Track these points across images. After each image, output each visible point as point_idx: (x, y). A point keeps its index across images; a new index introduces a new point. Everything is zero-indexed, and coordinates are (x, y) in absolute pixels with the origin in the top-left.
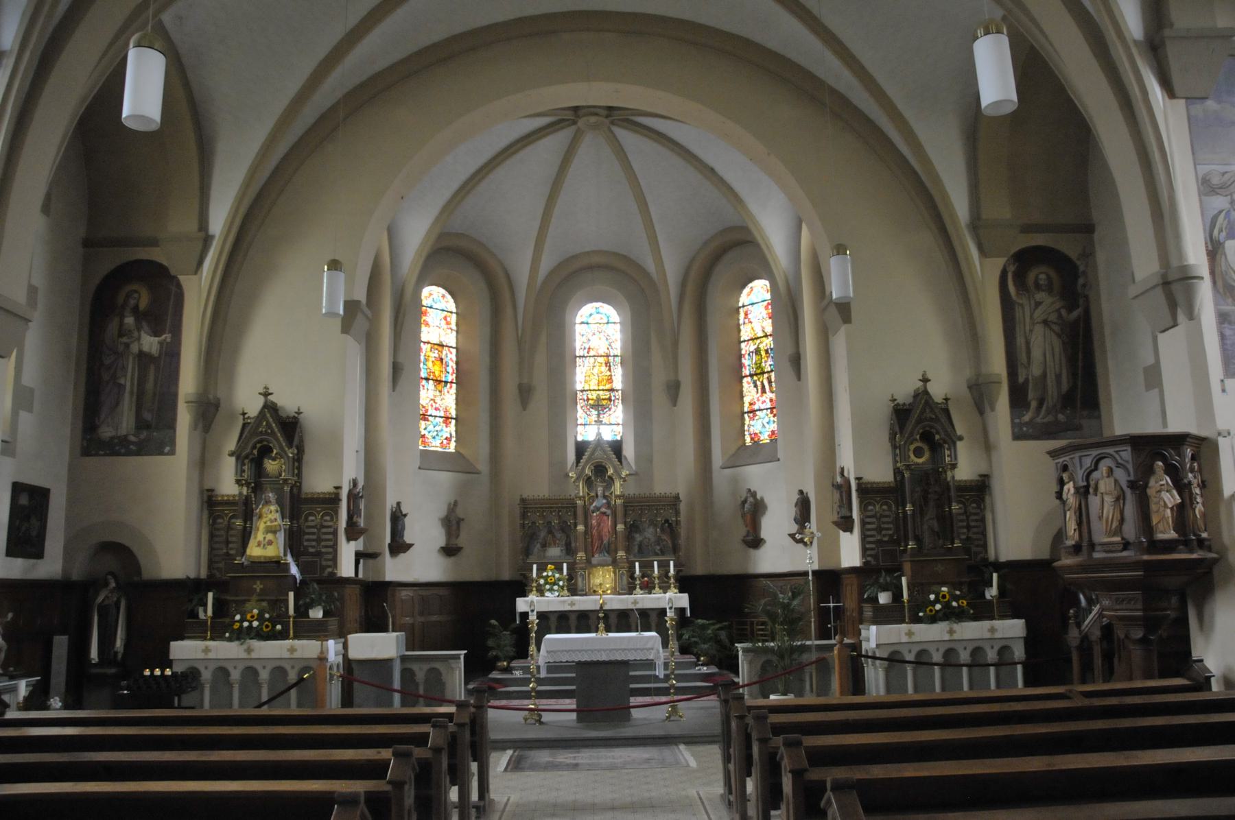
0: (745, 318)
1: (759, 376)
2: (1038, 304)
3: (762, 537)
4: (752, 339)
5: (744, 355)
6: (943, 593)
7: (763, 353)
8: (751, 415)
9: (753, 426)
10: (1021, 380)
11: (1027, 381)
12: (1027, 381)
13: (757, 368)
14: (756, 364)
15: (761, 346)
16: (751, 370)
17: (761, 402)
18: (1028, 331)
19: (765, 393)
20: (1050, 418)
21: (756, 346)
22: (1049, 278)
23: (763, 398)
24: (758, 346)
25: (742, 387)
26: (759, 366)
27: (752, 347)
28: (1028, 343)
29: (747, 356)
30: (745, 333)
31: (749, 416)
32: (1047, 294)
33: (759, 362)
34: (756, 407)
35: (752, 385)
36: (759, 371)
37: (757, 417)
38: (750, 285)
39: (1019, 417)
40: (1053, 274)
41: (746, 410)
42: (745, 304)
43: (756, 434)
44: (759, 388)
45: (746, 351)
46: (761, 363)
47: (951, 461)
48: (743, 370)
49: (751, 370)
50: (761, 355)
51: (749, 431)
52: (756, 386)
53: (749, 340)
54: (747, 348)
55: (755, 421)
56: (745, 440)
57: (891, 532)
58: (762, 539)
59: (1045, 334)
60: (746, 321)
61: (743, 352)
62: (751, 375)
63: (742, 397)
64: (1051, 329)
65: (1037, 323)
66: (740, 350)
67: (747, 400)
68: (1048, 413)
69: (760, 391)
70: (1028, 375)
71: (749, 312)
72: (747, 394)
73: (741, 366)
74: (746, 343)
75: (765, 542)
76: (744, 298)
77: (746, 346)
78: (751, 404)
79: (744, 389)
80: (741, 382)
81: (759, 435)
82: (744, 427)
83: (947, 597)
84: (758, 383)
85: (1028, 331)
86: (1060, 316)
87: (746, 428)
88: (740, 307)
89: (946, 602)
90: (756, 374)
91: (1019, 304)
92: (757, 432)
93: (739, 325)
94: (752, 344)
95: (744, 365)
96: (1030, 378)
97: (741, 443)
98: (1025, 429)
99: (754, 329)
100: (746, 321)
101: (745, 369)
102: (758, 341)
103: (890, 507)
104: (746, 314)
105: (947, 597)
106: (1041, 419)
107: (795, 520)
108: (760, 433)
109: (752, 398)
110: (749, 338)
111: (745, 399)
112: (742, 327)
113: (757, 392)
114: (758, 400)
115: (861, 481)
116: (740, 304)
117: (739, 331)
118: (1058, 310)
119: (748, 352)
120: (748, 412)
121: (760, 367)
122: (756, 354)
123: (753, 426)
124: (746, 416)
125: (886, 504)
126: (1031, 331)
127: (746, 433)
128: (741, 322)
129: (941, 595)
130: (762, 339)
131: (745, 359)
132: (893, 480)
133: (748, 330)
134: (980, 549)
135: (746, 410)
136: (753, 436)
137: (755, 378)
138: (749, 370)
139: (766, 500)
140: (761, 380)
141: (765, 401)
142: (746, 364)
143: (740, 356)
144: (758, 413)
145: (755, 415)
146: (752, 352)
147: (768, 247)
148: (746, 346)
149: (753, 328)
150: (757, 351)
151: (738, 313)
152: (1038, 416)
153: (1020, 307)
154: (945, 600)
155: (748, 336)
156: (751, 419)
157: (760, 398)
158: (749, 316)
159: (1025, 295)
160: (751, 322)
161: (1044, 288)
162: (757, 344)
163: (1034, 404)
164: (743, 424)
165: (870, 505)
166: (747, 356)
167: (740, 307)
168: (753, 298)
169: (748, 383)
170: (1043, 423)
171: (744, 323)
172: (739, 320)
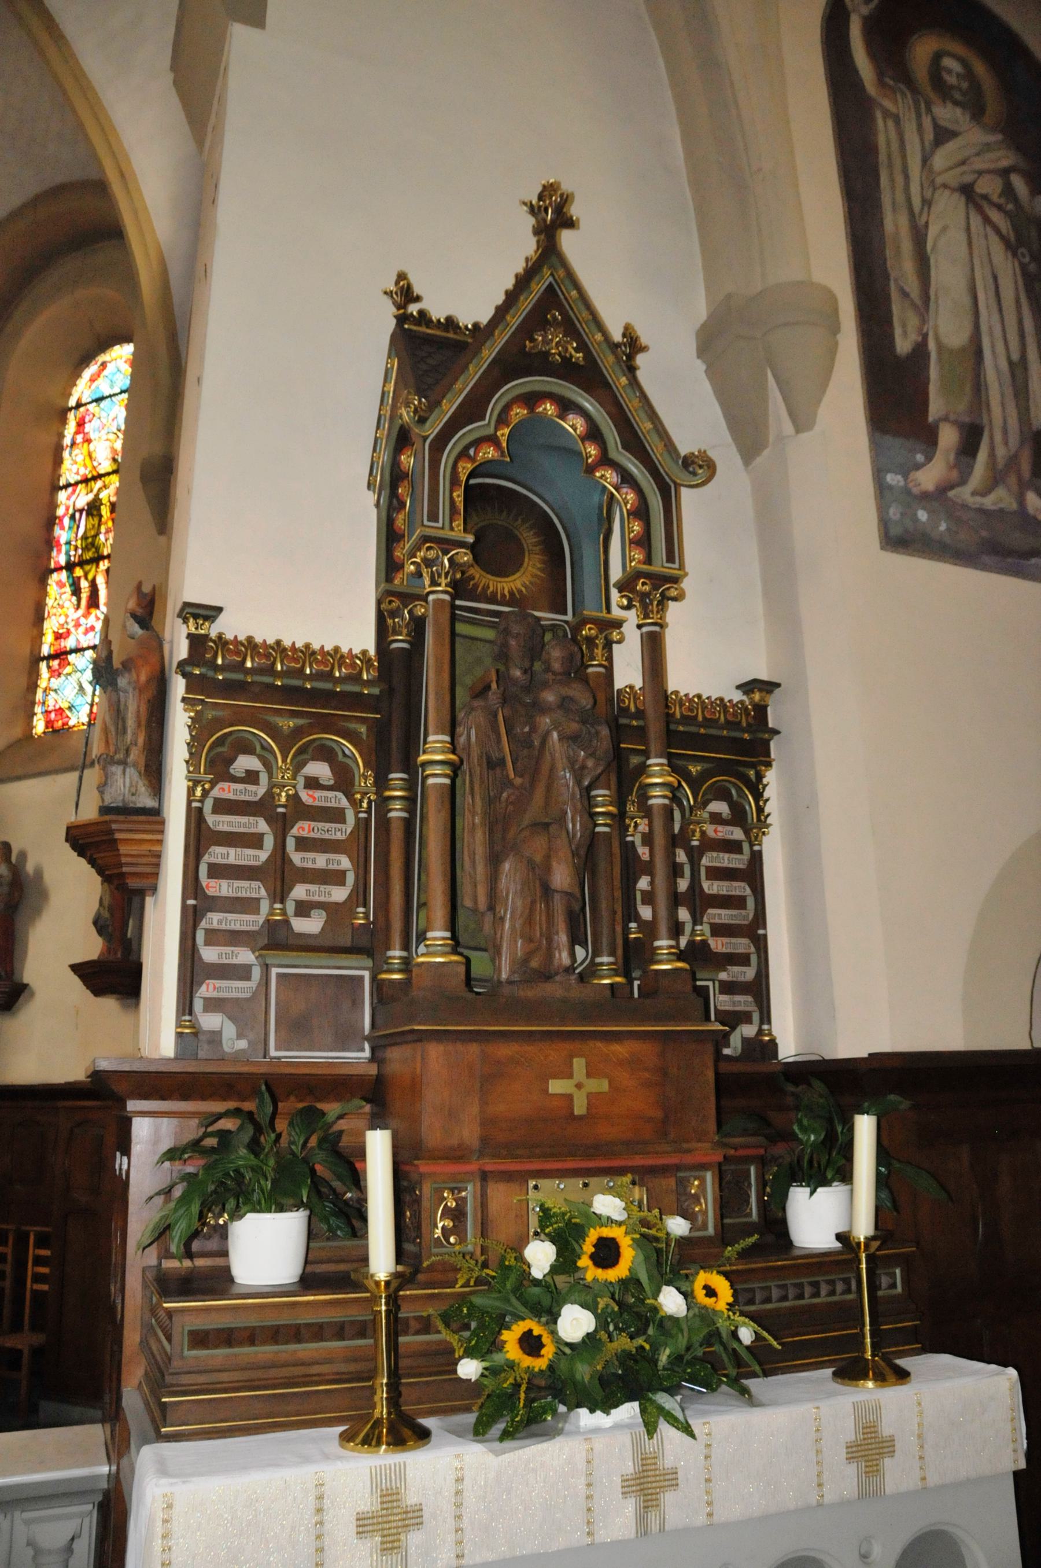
0: (77, 433)
1: (87, 568)
2: (943, 135)
3: (25, 981)
4: (86, 481)
5: (61, 519)
6: (606, 1232)
7: (105, 511)
8: (55, 663)
9: (55, 691)
10: (903, 345)
11: (920, 351)
12: (920, 351)
13: (85, 549)
14: (85, 537)
15: (104, 495)
16: (72, 553)
17: (82, 629)
18: (917, 202)
19: (97, 606)
20: (1000, 498)
21: (91, 497)
22: (969, 74)
23: (91, 620)
24: (97, 495)
25: (45, 594)
26: (90, 542)
27: (82, 498)
28: (919, 236)
29: (66, 521)
30: (71, 469)
31: (49, 667)
32: (968, 117)
33: (93, 533)
34: (70, 643)
35: (68, 589)
36: (89, 555)
37: (68, 669)
38: (102, 358)
39: (907, 470)
40: (980, 68)
41: (45, 650)
42: (84, 401)
43: (60, 711)
44: (85, 596)
45: (67, 509)
46: (98, 534)
47: (648, 560)
48: (54, 553)
49: (72, 553)
50: (101, 516)
51: (44, 703)
52: (76, 591)
53: (76, 484)
54: (71, 503)
55: (63, 677)
56: (32, 728)
57: (339, 894)
58: (25, 986)
59: (968, 224)
60: (79, 438)
61: (60, 512)
62: (70, 567)
63: (39, 618)
64: (987, 220)
65: (945, 186)
66: (53, 505)
67: (50, 627)
68: (995, 479)
69: (84, 602)
70: (925, 336)
71: (87, 419)
72: (53, 611)
73: (50, 543)
74: (70, 489)
75: (32, 994)
76: (82, 390)
77: (68, 498)
78: (58, 636)
79: (49, 602)
80: (43, 582)
81: (68, 712)
82: (35, 693)
83: (628, 1254)
84: (84, 584)
85: (917, 202)
86: (1009, 191)
87: (39, 695)
88: (70, 409)
89: (623, 1282)
90: (81, 563)
91: (887, 114)
92: (65, 705)
93: (59, 449)
94: (84, 492)
95: (58, 542)
96: (932, 345)
97: (17, 732)
98: (922, 515)
99: (94, 455)
100: (79, 438)
101: (59, 551)
102: (99, 484)
103: (344, 782)
104: (81, 424)
105: (628, 1254)
106: (974, 493)
107: (95, 923)
108: (70, 708)
109: (62, 620)
110: (79, 478)
111: (47, 625)
112: (66, 454)
113: (78, 606)
114: (78, 625)
115: (214, 630)
116: (72, 402)
117: (58, 461)
118: (1005, 173)
119: (71, 511)
120: (50, 657)
121: (93, 544)
122: (88, 515)
123: (55, 691)
124: (43, 666)
125: (326, 754)
126: (927, 203)
127: (38, 709)
128: (67, 441)
129: (588, 1248)
130: (107, 479)
131: (62, 528)
132: (371, 647)
133: (80, 459)
134: (743, 1002)
135: (45, 650)
136: (53, 715)
137: (78, 572)
138: (67, 553)
139: (48, 878)
140: (90, 577)
141: (92, 628)
142: (63, 541)
143: (51, 521)
144: (71, 658)
145: (64, 663)
146: (81, 511)
147: (122, 175)
148: (68, 498)
149: (90, 455)
150: (93, 509)
151: (64, 421)
152: (963, 481)
153: (890, 124)
154: (612, 1275)
155: (77, 473)
156: (55, 673)
157: (83, 621)
158: (88, 428)
159: (903, 94)
160: (88, 441)
161: (958, 96)
162: (95, 491)
163: (948, 437)
164: (33, 687)
165: (246, 747)
166: (66, 521)
167: (70, 409)
168: (104, 387)
169: (60, 584)
170: (982, 511)
171: (73, 444)
172: (61, 436)
